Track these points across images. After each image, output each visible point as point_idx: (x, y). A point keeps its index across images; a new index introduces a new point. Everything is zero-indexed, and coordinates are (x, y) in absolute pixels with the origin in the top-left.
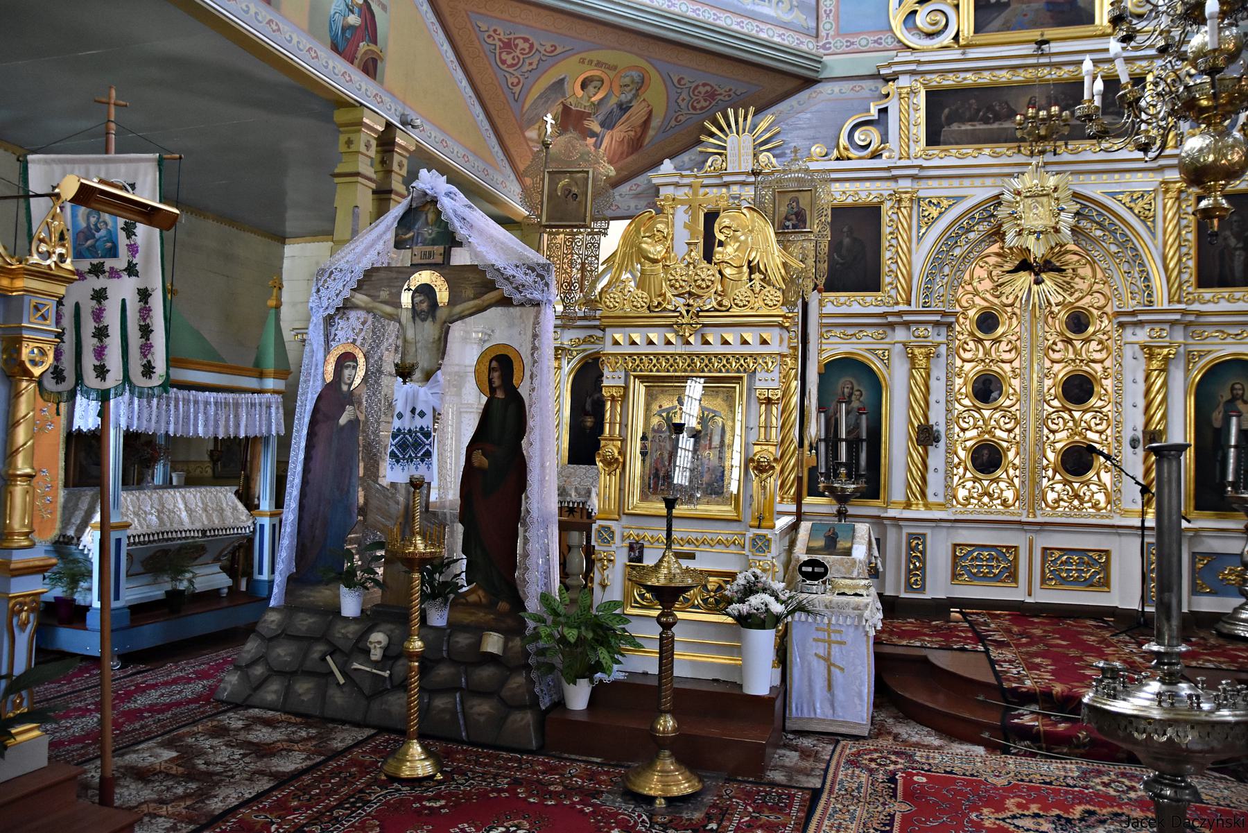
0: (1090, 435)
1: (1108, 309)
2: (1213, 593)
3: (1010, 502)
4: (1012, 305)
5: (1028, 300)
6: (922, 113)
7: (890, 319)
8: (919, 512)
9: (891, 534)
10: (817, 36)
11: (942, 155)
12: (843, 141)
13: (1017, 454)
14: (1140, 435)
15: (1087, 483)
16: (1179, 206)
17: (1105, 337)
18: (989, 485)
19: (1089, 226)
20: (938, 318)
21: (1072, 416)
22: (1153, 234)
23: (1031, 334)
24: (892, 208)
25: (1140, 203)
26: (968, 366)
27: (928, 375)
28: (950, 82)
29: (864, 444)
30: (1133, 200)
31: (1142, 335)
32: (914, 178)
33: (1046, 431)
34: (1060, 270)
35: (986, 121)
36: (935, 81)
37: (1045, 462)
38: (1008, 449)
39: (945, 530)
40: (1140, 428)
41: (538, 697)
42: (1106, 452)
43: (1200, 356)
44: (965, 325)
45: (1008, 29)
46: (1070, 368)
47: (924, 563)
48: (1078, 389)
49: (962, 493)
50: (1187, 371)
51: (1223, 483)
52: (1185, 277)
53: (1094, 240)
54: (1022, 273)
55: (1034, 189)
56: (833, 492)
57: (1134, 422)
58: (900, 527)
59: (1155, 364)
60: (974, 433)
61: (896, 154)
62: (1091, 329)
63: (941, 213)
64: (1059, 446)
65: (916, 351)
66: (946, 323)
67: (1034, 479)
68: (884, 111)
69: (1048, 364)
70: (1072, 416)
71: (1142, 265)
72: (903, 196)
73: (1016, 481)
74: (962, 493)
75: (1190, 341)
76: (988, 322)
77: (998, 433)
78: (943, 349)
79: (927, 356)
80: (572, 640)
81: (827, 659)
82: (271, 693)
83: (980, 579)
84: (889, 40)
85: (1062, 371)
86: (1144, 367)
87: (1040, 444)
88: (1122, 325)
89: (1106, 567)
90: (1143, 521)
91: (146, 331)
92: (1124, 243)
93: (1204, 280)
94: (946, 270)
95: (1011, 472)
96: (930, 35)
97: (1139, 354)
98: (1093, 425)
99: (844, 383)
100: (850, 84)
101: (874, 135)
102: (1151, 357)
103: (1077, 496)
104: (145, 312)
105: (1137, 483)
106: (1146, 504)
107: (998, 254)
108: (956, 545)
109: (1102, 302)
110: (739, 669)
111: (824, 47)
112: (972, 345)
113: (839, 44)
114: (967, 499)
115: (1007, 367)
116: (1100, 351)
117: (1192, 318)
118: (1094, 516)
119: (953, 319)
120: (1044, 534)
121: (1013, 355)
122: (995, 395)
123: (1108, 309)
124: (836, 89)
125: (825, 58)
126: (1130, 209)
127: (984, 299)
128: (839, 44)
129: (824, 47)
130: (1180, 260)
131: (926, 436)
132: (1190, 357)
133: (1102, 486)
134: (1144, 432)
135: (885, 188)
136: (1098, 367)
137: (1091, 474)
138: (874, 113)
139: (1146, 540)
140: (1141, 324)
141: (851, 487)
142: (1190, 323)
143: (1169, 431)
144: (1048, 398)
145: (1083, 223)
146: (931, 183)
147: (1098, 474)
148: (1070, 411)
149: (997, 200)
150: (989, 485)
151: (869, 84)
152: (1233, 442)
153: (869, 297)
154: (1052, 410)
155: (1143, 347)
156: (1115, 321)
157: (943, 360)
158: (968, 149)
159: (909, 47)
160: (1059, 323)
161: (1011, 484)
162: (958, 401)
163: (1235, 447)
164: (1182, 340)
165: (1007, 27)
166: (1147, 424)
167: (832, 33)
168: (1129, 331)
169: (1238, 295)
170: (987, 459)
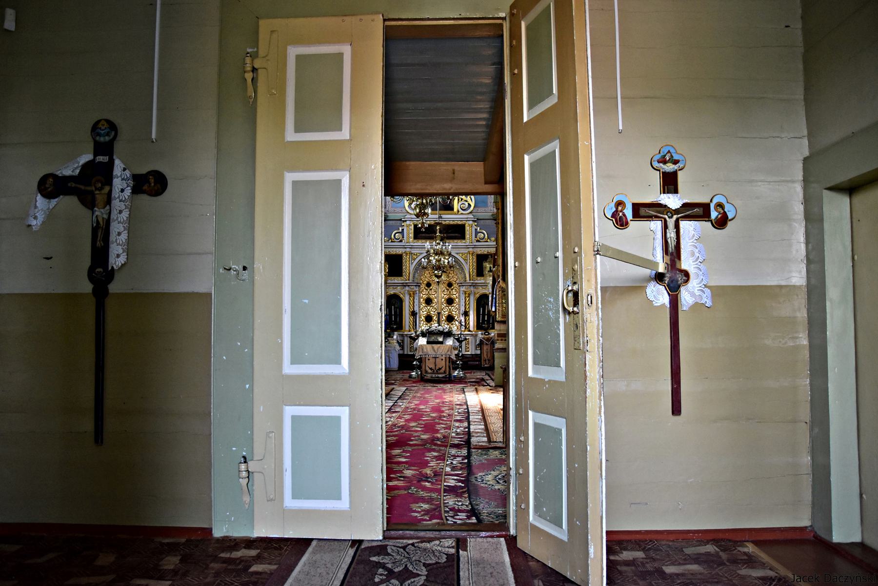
41: (432, 408)
44: (423, 286)
66: (418, 285)
76: (429, 285)
80: (13, 29)
92: (460, 266)
131: (414, 314)
135: (403, 250)
142: (475, 285)
153: (399, 278)
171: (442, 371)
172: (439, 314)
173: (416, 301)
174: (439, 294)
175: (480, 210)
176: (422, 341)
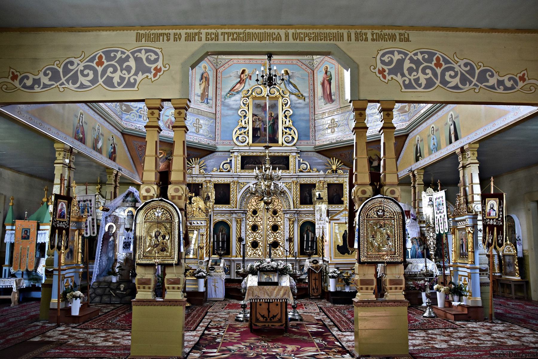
6: (240, 161)
9: (233, 264)
12: (221, 167)
26: (250, 223)
31: (288, 216)
36: (243, 154)
44: (250, 213)
48: (275, 228)
56: (218, 254)
57: (287, 236)
68: (231, 160)
76: (255, 212)
78: (244, 219)
79: (240, 221)
81: (215, 286)
82: (97, 299)
88: (284, 213)
91: (93, 226)
93: (302, 203)
96: (242, 142)
99: (221, 227)
100: (223, 153)
102: (290, 221)
103: (255, 253)
104: (93, 223)
110: (197, 288)
131: (240, 240)
136: (279, 223)
138: (228, 161)
142: (298, 213)
151: (227, 153)
153: (227, 206)
165: (259, 142)
170: (255, 245)
171: (276, 319)
172: (163, 194)
173: (243, 228)
174: (265, 221)
175: (303, 142)
176: (252, 281)
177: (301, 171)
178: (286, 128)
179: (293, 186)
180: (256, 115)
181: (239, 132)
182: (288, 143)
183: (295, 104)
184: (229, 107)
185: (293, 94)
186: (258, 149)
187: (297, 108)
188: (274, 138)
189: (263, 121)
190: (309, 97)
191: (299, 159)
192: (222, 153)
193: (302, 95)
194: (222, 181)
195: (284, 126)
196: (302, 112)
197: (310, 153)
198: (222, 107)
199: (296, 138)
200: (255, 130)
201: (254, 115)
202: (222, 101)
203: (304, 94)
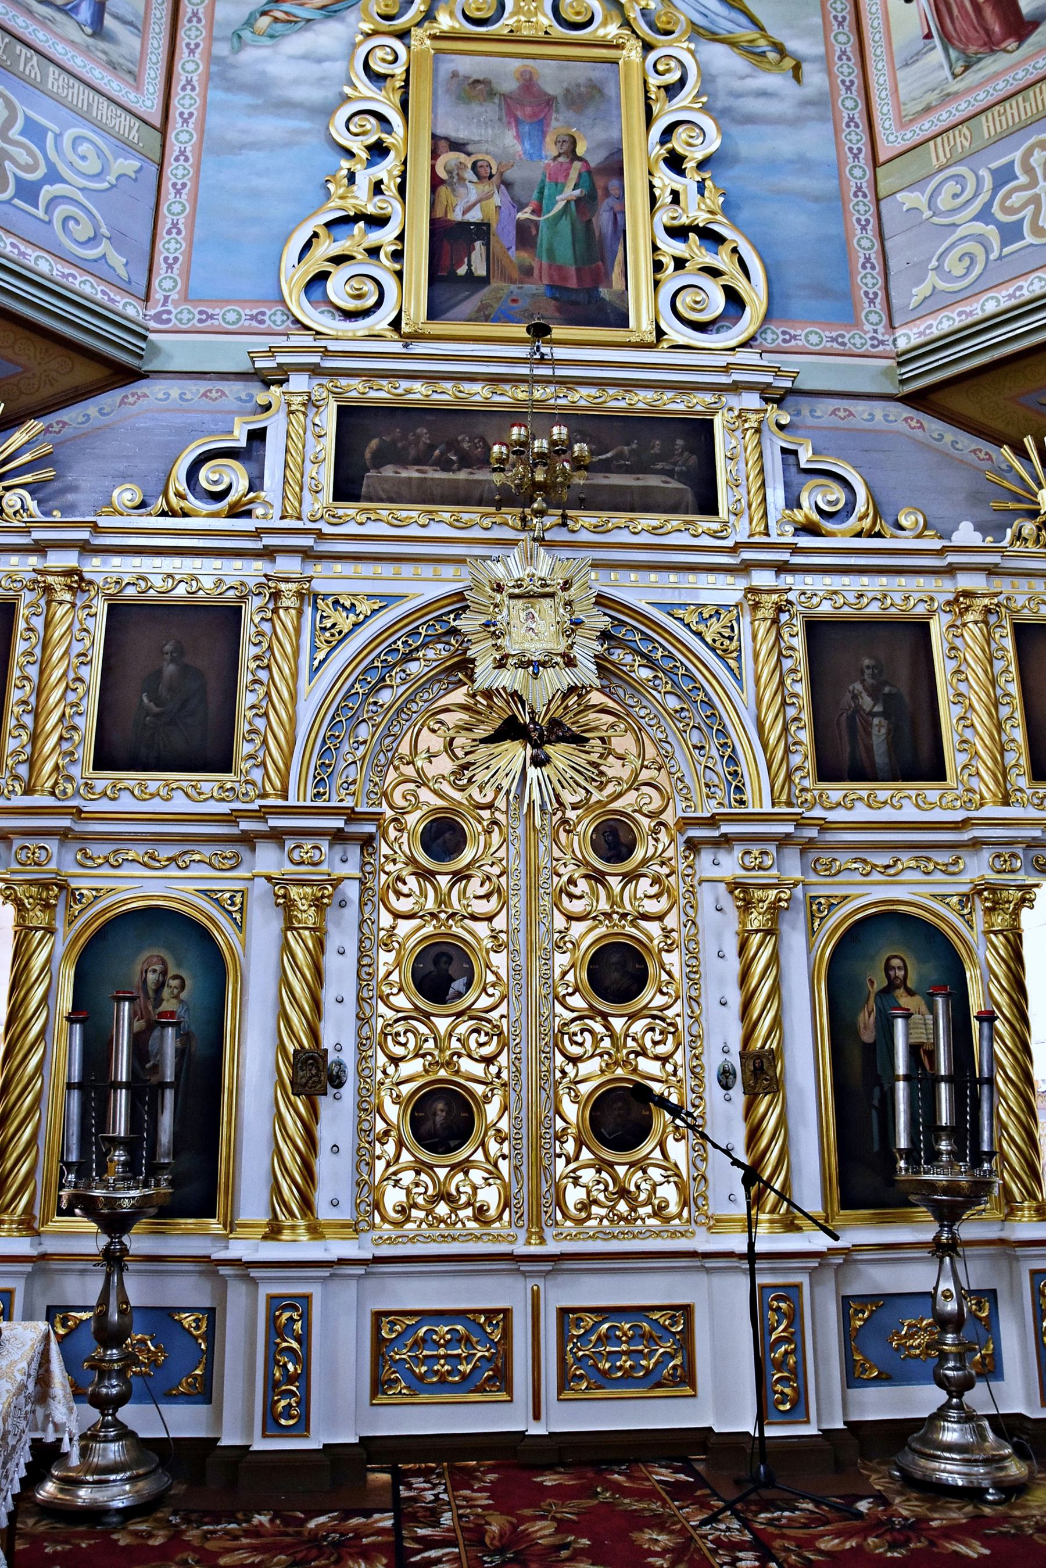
0: (645, 1065)
1: (668, 817)
2: (885, 1379)
3: (493, 1212)
4: (490, 806)
5: (519, 797)
7: (245, 825)
8: (299, 1247)
9: (237, 1296)
10: (147, 299)
11: (363, 518)
12: (179, 482)
13: (505, 1108)
14: (736, 1062)
15: (641, 1166)
16: (779, 636)
17: (665, 870)
18: (449, 1177)
19: (629, 659)
20: (339, 823)
21: (608, 1027)
22: (739, 680)
23: (528, 863)
24: (261, 609)
25: (715, 626)
26: (404, 927)
27: (320, 944)
28: (382, 394)
29: (169, 1095)
30: (702, 620)
31: (729, 865)
32: (307, 554)
33: (559, 1059)
34: (578, 740)
35: (445, 465)
36: (355, 389)
37: (560, 1124)
38: (487, 1099)
39: (353, 1283)
40: (736, 1047)
42: (674, 1099)
43: (831, 906)
44: (402, 845)
45: (487, 319)
46: (602, 930)
47: (305, 1361)
49: (393, 1197)
50: (812, 932)
51: (888, 1152)
52: (796, 760)
53: (637, 688)
54: (507, 744)
55: (531, 591)
56: (90, 1208)
57: (724, 1037)
58: (254, 1282)
59: (756, 920)
60: (415, 1066)
61: (276, 512)
62: (639, 854)
63: (357, 625)
64: (584, 1089)
65: (294, 892)
67: (539, 1160)
68: (258, 436)
69: (560, 922)
70: (608, 1027)
71: (723, 732)
72: (283, 586)
73: (504, 1166)
74: (393, 1197)
75: (813, 878)
76: (443, 836)
77: (466, 1065)
78: (352, 891)
79: (318, 904)
83: (432, 1388)
84: (279, 318)
85: (586, 936)
86: (737, 927)
87: (550, 1086)
88: (693, 846)
89: (686, 1342)
90: (751, 1245)
93: (827, 771)
94: (363, 732)
95: (493, 1147)
97: (728, 903)
98: (648, 1044)
99: (145, 962)
100: (203, 386)
101: (234, 476)
102: (746, 906)
103: (623, 1193)
105: (736, 1163)
106: (755, 1202)
107: (465, 708)
108: (378, 1315)
109: (657, 803)
111: (157, 318)
112: (412, 882)
113: (185, 316)
114: (402, 1210)
115: (482, 929)
116: (657, 896)
117: (813, 833)
118: (658, 1234)
119: (370, 828)
120: (562, 1279)
121: (493, 904)
122: (458, 985)
123: (668, 817)
124: (175, 393)
125: (152, 336)
126: (698, 634)
127: (435, 792)
128: (185, 316)
129: (157, 318)
130: (785, 729)
132: (816, 910)
133: (672, 1171)
134: (742, 1055)
136: (653, 928)
137: (648, 1147)
138: (240, 439)
139: (760, 1280)
140: (725, 842)
141: (130, 1195)
142: (809, 842)
143: (787, 1055)
144: (562, 991)
145: (618, 655)
146: (338, 567)
147: (662, 1145)
148: (605, 1016)
149: (459, 602)
150: (449, 1177)
151: (236, 389)
152: (901, 1069)
153: (209, 782)
154: (569, 1015)
155: (733, 886)
156: (681, 839)
157: (351, 913)
158: (411, 512)
159: (307, 328)
160: (579, 842)
161: (494, 1173)
162: (385, 999)
163: (907, 1078)
164: (798, 876)
165: (483, 316)
166: (747, 1039)
167: (174, 296)
168: (706, 857)
169: (883, 795)
170: (443, 1120)
175: (808, 335)
177: (809, 529)
178: (678, 233)
179: (753, 635)
180: (456, 146)
181: (327, 248)
182: (701, 327)
183: (738, 95)
184: (265, 96)
185: (714, 37)
186: (476, 361)
187: (750, 119)
188: (592, 293)
189: (508, 185)
190: (826, 61)
191: (783, 441)
192: (194, 388)
193: (780, 49)
194: (164, 578)
195: (664, 217)
196: (785, 144)
197: (861, 408)
198: (216, 95)
199: (756, 295)
200: (448, 238)
201: (439, 144)
202: (210, 59)
203: (792, 45)
